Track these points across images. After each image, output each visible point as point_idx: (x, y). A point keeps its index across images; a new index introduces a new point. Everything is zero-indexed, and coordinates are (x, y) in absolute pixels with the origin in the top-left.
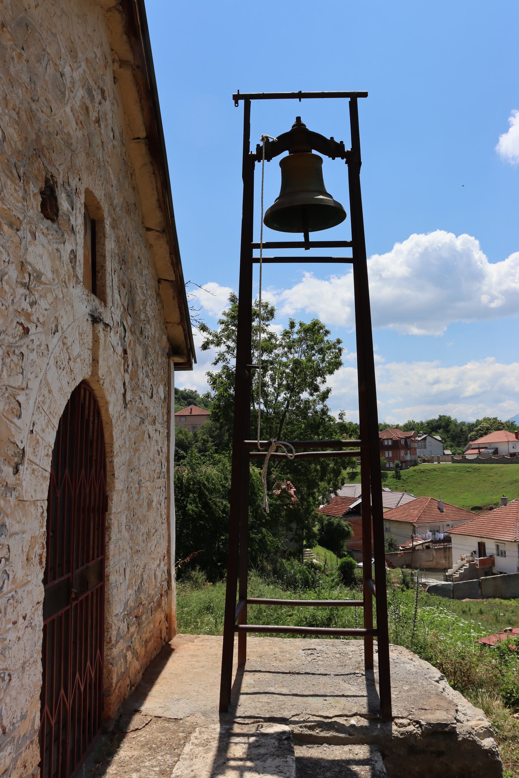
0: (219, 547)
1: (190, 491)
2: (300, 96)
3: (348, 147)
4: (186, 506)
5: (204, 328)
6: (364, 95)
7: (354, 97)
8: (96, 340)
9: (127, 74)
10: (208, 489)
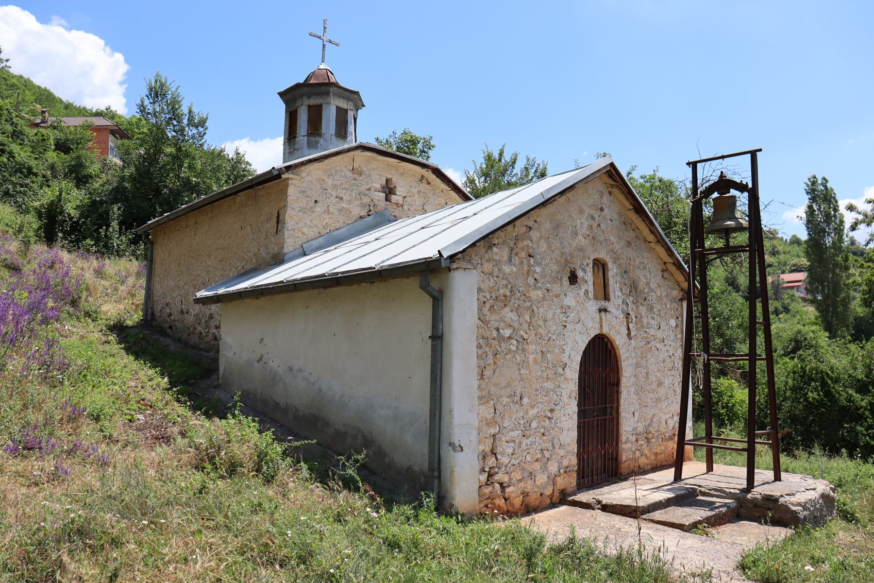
0: (843, 434)
1: (812, 380)
2: (723, 157)
3: (750, 186)
4: (807, 394)
5: (851, 208)
6: (760, 150)
7: (753, 154)
8: (601, 319)
9: (615, 191)
10: (831, 378)
